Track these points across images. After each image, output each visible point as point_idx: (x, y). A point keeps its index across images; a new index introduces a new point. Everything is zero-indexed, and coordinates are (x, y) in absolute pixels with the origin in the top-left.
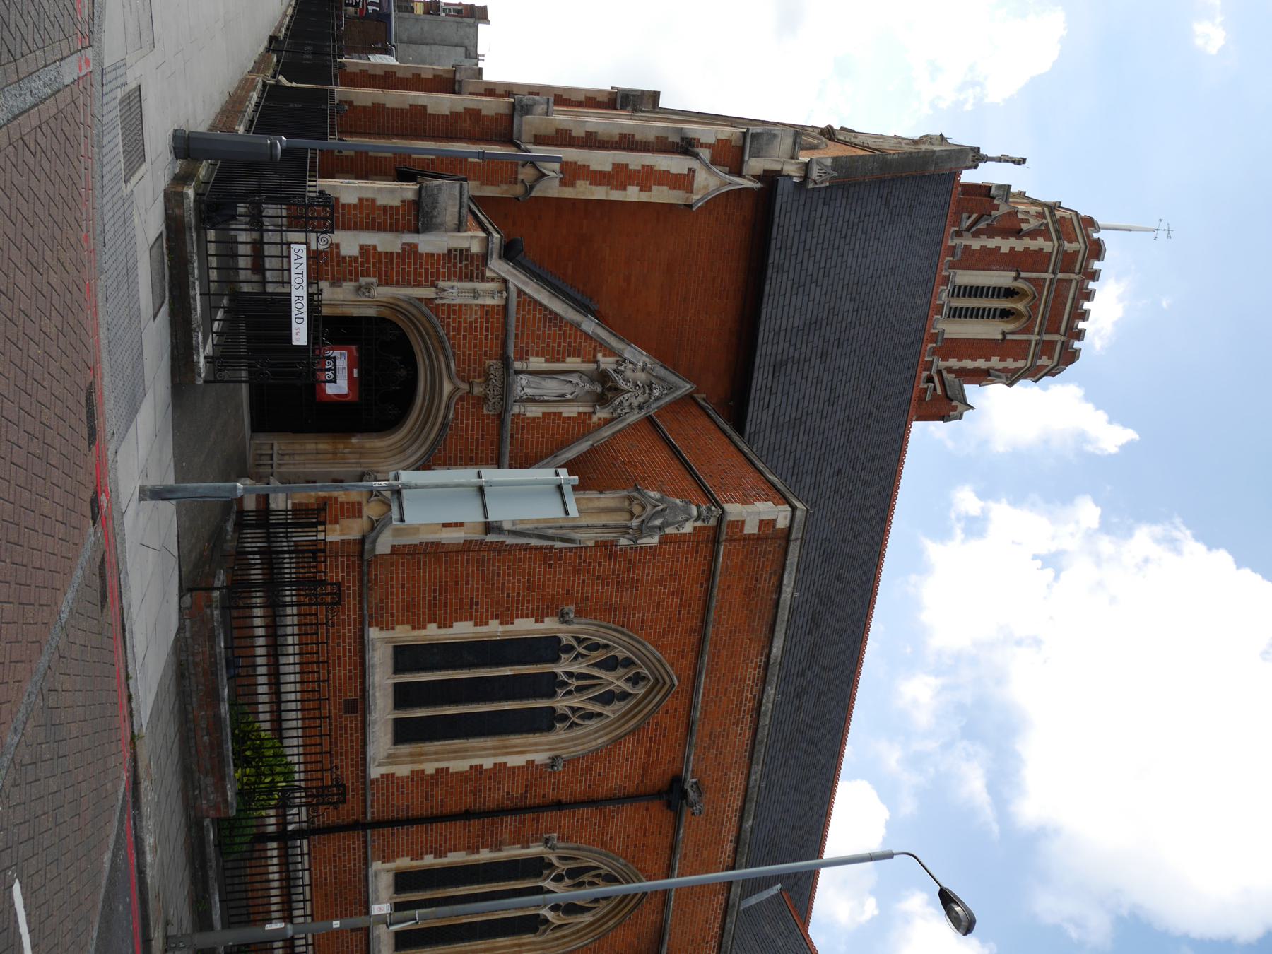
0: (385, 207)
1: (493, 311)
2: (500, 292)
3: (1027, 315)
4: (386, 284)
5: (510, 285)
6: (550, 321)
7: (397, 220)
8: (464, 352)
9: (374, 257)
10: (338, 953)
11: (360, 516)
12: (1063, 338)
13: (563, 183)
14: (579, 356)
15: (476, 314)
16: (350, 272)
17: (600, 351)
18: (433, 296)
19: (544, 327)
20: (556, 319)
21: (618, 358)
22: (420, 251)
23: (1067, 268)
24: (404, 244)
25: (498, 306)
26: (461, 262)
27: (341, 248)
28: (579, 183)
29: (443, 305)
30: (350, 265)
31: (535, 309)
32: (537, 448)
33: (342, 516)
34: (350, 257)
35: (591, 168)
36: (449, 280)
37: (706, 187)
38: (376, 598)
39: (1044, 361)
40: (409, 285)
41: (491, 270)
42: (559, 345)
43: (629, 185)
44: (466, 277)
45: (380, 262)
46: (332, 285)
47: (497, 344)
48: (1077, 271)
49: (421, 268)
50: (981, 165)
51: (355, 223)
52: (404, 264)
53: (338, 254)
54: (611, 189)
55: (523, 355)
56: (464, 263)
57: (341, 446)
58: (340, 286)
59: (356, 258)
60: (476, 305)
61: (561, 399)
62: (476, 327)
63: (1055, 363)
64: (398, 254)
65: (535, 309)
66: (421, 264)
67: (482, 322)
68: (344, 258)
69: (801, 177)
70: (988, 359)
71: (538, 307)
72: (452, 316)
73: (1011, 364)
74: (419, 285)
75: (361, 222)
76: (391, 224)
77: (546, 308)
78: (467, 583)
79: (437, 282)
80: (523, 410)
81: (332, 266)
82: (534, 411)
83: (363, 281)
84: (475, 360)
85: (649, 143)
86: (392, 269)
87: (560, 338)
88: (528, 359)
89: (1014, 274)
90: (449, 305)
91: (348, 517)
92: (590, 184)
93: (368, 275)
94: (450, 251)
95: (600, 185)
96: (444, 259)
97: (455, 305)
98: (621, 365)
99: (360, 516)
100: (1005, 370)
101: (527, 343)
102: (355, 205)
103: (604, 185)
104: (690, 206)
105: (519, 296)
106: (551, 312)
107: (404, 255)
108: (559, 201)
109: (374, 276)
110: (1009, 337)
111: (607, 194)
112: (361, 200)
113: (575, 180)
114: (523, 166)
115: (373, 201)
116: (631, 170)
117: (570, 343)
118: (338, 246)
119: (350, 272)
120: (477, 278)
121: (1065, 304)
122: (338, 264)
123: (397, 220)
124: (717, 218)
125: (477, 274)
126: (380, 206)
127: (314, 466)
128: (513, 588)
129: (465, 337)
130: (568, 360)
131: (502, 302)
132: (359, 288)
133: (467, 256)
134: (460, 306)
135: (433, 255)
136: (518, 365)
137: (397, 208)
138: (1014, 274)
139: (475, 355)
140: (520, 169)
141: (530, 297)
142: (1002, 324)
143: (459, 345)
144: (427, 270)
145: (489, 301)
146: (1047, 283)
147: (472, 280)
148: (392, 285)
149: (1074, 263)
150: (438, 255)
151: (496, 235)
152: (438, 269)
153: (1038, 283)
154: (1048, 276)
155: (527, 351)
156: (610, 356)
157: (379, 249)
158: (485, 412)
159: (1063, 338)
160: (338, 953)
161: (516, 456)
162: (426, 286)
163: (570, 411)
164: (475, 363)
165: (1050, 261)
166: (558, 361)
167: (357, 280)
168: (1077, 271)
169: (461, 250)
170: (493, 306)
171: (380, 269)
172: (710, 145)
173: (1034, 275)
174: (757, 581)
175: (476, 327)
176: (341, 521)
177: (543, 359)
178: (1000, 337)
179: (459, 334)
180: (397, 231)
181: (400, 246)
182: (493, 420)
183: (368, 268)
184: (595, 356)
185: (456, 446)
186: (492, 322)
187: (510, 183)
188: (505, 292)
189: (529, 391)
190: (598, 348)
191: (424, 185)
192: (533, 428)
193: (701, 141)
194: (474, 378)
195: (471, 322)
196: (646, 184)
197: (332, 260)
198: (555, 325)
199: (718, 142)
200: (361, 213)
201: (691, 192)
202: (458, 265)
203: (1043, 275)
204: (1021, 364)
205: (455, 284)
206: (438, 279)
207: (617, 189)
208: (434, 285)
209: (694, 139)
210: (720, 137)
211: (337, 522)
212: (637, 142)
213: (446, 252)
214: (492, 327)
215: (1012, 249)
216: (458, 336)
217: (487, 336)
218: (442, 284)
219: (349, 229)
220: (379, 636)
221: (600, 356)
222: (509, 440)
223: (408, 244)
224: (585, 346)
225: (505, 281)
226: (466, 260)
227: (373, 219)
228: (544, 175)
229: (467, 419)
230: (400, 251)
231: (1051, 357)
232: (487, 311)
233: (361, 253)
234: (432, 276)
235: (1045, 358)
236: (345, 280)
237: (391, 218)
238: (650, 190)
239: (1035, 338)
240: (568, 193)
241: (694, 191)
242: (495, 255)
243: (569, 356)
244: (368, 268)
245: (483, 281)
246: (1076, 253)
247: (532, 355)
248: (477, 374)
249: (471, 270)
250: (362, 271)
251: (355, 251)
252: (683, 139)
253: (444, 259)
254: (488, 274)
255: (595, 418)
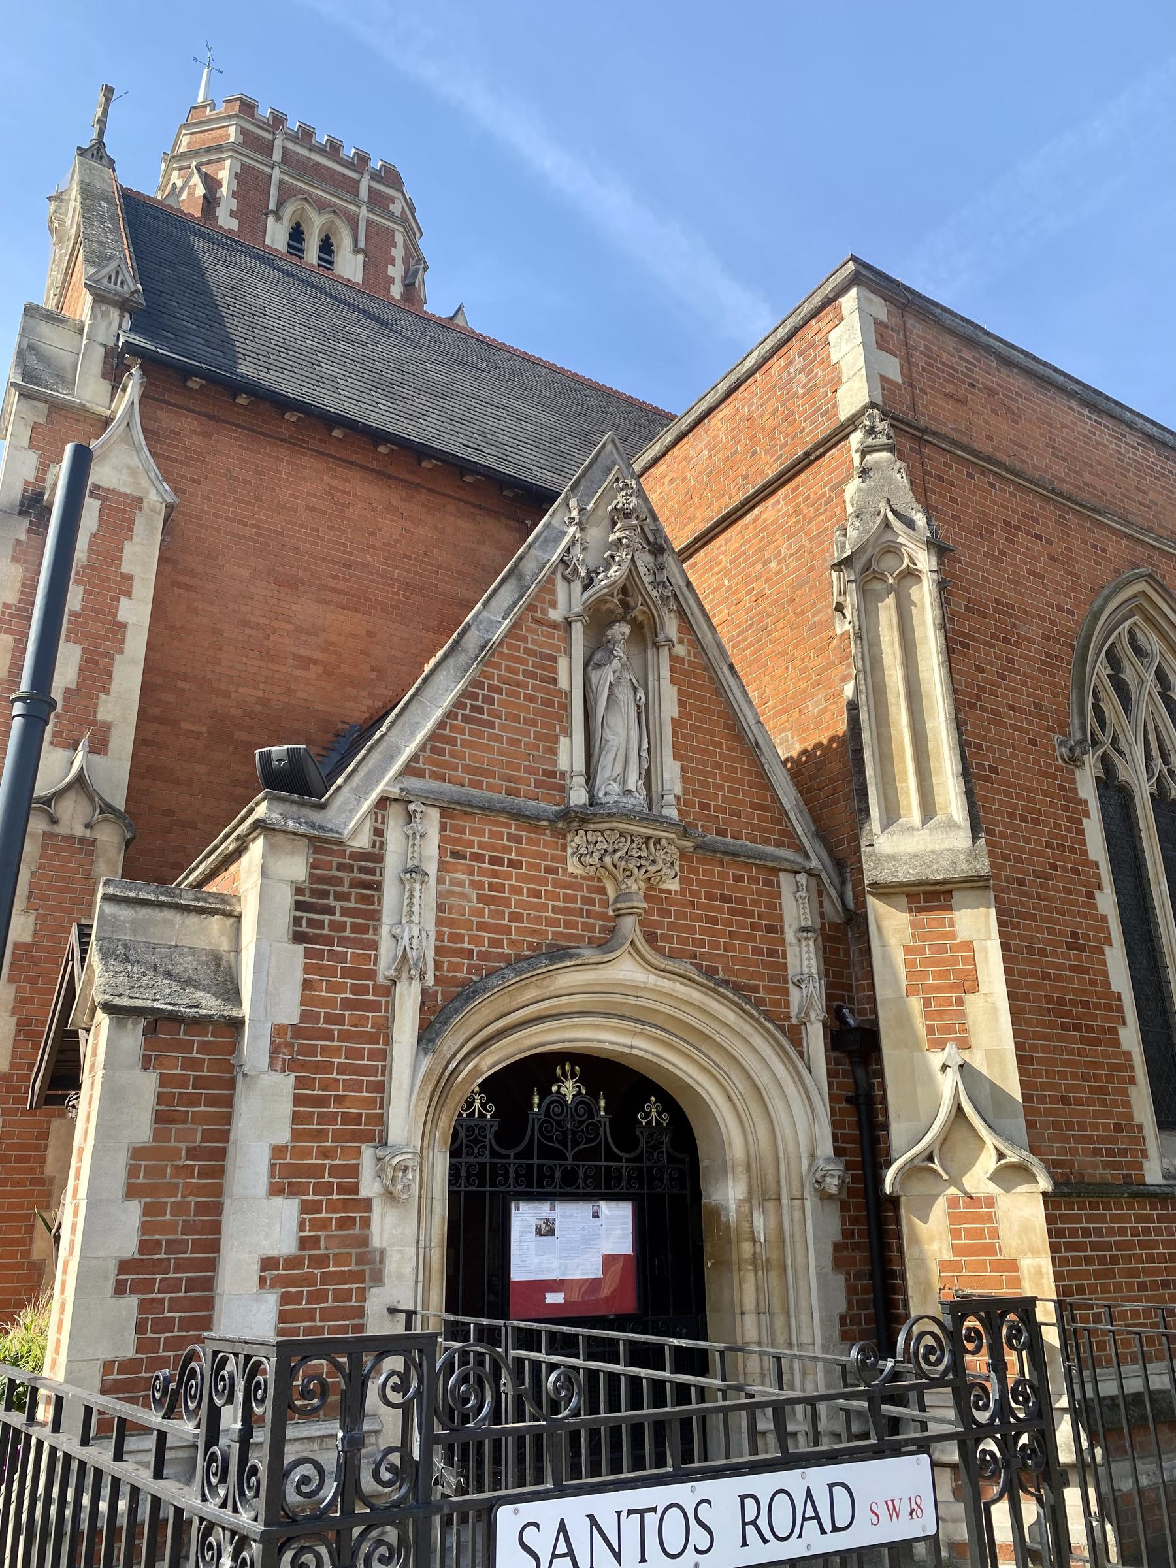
0: (160, 1118)
1: (455, 841)
2: (410, 817)
3: (332, 215)
4: (381, 1120)
5: (395, 791)
6: (480, 710)
7: (199, 1082)
8: (551, 922)
9: (306, 1153)
10: (1173, 1258)
11: (990, 1201)
12: (367, 177)
13: (99, 746)
14: (554, 659)
15: (461, 884)
16: (343, 1223)
17: (544, 612)
18: (416, 987)
19: (491, 725)
20: (474, 696)
21: (559, 576)
22: (295, 1020)
23: (266, 148)
24: (272, 1064)
25: (443, 827)
26: (330, 911)
27: (274, 1253)
28: (102, 715)
29: (438, 965)
30: (324, 1224)
31: (452, 741)
32: (741, 782)
33: (990, 1249)
34: (302, 1226)
35: (73, 686)
36: (374, 946)
37: (133, 472)
38: (1094, 1166)
39: (396, 208)
40: (383, 1055)
41: (355, 832)
42: (532, 699)
43: (115, 615)
44: (368, 900)
45: (320, 1135)
46: (378, 1279)
47: (530, 841)
48: (270, 137)
49: (339, 1020)
50: (110, 151)
51: (201, 1208)
52: (326, 1067)
53: (292, 1262)
54: (121, 652)
55: (555, 782)
56: (331, 902)
57: (747, 1247)
58: (382, 1252)
59: (306, 1207)
60: (441, 881)
61: (643, 713)
62: (492, 887)
63: (399, 195)
64: (299, 1083)
65: (452, 741)
66: (329, 1019)
67: (482, 872)
68: (303, 1243)
69: (122, 316)
70: (391, 280)
71: (447, 732)
72: (466, 945)
73: (398, 253)
74: (384, 1032)
75: (199, 1190)
76: (212, 1101)
77: (450, 715)
78: (1043, 952)
79: (381, 980)
80: (670, 799)
81: (327, 1278)
82: (671, 775)
83: (369, 1187)
84: (566, 898)
85: (24, 577)
86: (339, 1100)
87: (516, 695)
88: (563, 774)
89: (271, 219)
90: (439, 951)
91: (995, 1233)
92: (106, 691)
93: (355, 1171)
94: (298, 938)
95: (110, 673)
96: (319, 955)
97: (440, 937)
98: (576, 570)
99: (990, 1201)
100: (406, 261)
101: (529, 770)
102: (147, 1210)
103: (112, 665)
104: (170, 508)
105: (420, 774)
106: (458, 704)
107: (303, 1066)
108: (139, 770)
109: (359, 1151)
110: (362, 244)
111: (133, 662)
112: (132, 1192)
113: (94, 722)
114: (54, 821)
115: (137, 1153)
116: (83, 608)
117: (526, 673)
118: (268, 1264)
119: (343, 1223)
120: (372, 872)
121: (317, 164)
122: (321, 1261)
123: (199, 1082)
124: (194, 481)
125: (362, 870)
126: (157, 1135)
127: (804, 1319)
128: (1040, 854)
129: (515, 917)
130: (563, 683)
131: (434, 814)
132: (389, 1195)
133: (314, 893)
134: (440, 922)
135: (307, 984)
136: (578, 797)
137: (164, 1081)
138: (271, 219)
139: (555, 897)
140: (59, 830)
141: (422, 748)
142: (341, 252)
143: (532, 933)
144: (347, 1004)
145: (431, 848)
146: (287, 178)
147: (378, 887)
148: (383, 1103)
149: (258, 138)
150: (307, 969)
151: (261, 811)
152: (346, 973)
153: (286, 193)
154: (276, 172)
155: (546, 773)
156: (553, 592)
157: (283, 1136)
158: (674, 885)
159: (367, 177)
160: (1173, 1258)
161: (759, 828)
162: (390, 1007)
163: (669, 705)
164: (573, 899)
165: (596, 1339)
166: (566, 706)
167: (367, 1204)
168: (270, 137)
169: (299, 906)
170: (442, 839)
171: (339, 1136)
172: (40, 463)
173: (274, 192)
174: (974, 386)
175: (492, 887)
176: (1007, 1254)
177: (564, 741)
178: (361, 257)
179: (508, 931)
180: (231, 1084)
181: (277, 1077)
182: (692, 870)
183: (335, 1171)
184: (554, 626)
185: (746, 961)
186: (481, 845)
187: (91, 853)
188: (411, 807)
189: (633, 781)
190: (539, 615)
191: (100, 998)
192: (705, 785)
193: (32, 479)
194: (605, 904)
195: (481, 899)
196: (116, 582)
197: (309, 1280)
198: (488, 700)
199: (37, 448)
200: (172, 1190)
201: (140, 500)
202: (338, 917)
203: (275, 181)
204: (399, 238)
205: (385, 930)
206: (372, 975)
207: (122, 642)
208: (388, 990)
209: (25, 490)
210: (25, 442)
211: (1013, 1265)
212: (20, 600)
213: (300, 948)
214: (493, 847)
215: (232, 214)
216: (475, 961)
217: (511, 863)
218: (385, 966)
219: (217, 1228)
220: (1158, 1162)
221: (555, 615)
222: (728, 840)
223: (274, 1051)
224: (534, 642)
225: (383, 802)
226: (325, 894)
227: (192, 1153)
228: (80, 779)
229: (692, 929)
230: (290, 1079)
231: (392, 200)
232: (455, 854)
233: (295, 1190)
234: (364, 990)
235: (392, 208)
236: (365, 1241)
237: (194, 1101)
238: (130, 578)
239: (363, 212)
240: (123, 741)
241: (139, 495)
242: (317, 817)
243: (554, 681)
244: (335, 1171)
245: (379, 858)
246: (243, 131)
247: (554, 763)
248: (597, 897)
249: (352, 885)
250: (342, 1189)
251: (289, 1208)
252: (22, 513)
253: (319, 955)
254: (363, 842)
255: (681, 650)
